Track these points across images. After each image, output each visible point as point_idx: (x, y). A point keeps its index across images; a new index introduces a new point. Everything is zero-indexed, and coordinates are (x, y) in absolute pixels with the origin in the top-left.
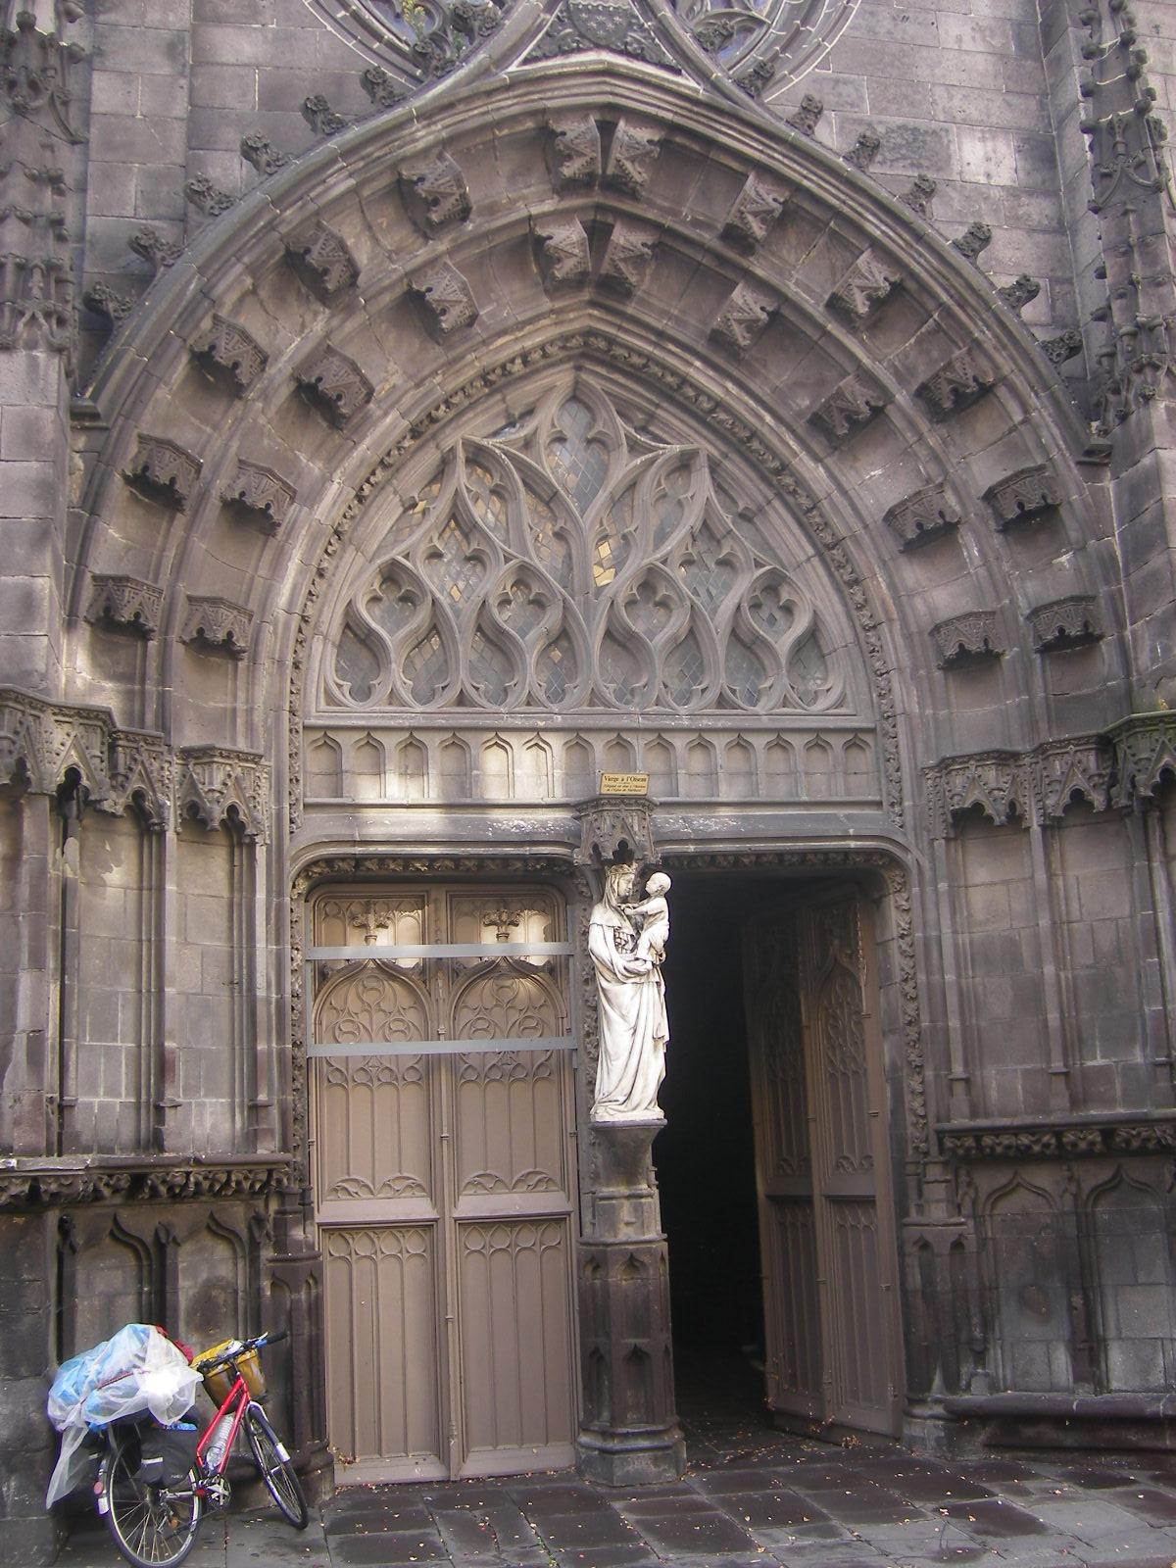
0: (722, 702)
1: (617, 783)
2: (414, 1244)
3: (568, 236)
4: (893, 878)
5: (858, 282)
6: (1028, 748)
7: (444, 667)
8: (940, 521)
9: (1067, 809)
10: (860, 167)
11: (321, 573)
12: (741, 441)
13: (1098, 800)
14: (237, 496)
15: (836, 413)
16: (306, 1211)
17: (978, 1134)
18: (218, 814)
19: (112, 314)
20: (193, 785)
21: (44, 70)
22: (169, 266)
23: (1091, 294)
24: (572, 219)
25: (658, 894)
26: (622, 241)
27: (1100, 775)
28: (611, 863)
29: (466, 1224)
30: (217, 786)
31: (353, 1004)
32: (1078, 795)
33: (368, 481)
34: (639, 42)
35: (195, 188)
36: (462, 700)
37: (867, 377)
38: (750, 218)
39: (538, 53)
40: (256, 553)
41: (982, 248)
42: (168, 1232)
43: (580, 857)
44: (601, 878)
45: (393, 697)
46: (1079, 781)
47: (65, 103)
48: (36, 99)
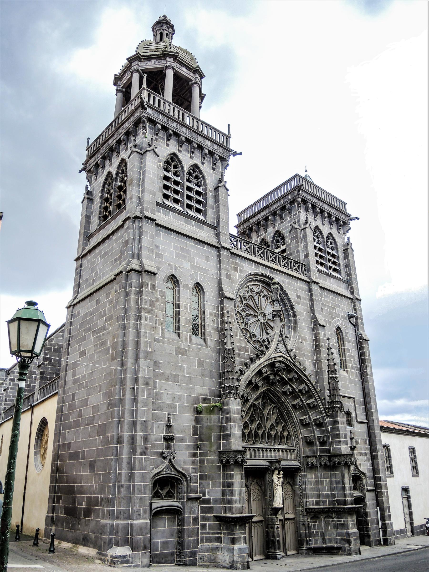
3: (272, 377)
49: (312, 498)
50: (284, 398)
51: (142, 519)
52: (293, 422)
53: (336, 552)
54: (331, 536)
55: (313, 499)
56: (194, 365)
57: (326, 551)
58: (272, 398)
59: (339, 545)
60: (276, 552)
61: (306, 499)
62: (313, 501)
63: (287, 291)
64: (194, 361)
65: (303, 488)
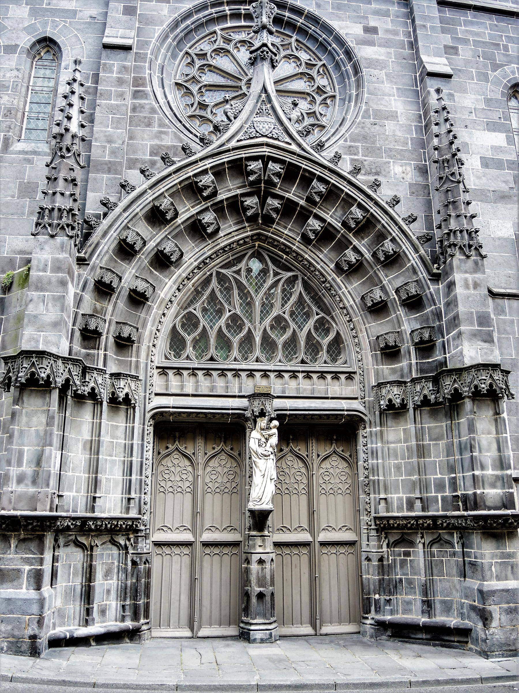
0: (303, 362)
3: (251, 201)
6: (409, 380)
11: (164, 314)
12: (312, 271)
17: (388, 518)
18: (122, 395)
21: (72, 144)
23: (437, 219)
25: (274, 427)
27: (433, 390)
28: (258, 417)
29: (206, 544)
30: (122, 386)
31: (170, 464)
32: (425, 396)
36: (212, 359)
37: (356, 250)
39: (243, 138)
41: (396, 204)
43: (248, 414)
44: (255, 422)
45: (188, 358)
46: (426, 392)
47: (79, 155)
49: (397, 491)
52: (344, 308)
53: (458, 642)
54: (448, 596)
55: (401, 495)
56: (10, 193)
57: (428, 637)
59: (467, 621)
60: (251, 624)
61: (379, 494)
62: (400, 499)
63: (327, 21)
64: (11, 185)
65: (370, 466)
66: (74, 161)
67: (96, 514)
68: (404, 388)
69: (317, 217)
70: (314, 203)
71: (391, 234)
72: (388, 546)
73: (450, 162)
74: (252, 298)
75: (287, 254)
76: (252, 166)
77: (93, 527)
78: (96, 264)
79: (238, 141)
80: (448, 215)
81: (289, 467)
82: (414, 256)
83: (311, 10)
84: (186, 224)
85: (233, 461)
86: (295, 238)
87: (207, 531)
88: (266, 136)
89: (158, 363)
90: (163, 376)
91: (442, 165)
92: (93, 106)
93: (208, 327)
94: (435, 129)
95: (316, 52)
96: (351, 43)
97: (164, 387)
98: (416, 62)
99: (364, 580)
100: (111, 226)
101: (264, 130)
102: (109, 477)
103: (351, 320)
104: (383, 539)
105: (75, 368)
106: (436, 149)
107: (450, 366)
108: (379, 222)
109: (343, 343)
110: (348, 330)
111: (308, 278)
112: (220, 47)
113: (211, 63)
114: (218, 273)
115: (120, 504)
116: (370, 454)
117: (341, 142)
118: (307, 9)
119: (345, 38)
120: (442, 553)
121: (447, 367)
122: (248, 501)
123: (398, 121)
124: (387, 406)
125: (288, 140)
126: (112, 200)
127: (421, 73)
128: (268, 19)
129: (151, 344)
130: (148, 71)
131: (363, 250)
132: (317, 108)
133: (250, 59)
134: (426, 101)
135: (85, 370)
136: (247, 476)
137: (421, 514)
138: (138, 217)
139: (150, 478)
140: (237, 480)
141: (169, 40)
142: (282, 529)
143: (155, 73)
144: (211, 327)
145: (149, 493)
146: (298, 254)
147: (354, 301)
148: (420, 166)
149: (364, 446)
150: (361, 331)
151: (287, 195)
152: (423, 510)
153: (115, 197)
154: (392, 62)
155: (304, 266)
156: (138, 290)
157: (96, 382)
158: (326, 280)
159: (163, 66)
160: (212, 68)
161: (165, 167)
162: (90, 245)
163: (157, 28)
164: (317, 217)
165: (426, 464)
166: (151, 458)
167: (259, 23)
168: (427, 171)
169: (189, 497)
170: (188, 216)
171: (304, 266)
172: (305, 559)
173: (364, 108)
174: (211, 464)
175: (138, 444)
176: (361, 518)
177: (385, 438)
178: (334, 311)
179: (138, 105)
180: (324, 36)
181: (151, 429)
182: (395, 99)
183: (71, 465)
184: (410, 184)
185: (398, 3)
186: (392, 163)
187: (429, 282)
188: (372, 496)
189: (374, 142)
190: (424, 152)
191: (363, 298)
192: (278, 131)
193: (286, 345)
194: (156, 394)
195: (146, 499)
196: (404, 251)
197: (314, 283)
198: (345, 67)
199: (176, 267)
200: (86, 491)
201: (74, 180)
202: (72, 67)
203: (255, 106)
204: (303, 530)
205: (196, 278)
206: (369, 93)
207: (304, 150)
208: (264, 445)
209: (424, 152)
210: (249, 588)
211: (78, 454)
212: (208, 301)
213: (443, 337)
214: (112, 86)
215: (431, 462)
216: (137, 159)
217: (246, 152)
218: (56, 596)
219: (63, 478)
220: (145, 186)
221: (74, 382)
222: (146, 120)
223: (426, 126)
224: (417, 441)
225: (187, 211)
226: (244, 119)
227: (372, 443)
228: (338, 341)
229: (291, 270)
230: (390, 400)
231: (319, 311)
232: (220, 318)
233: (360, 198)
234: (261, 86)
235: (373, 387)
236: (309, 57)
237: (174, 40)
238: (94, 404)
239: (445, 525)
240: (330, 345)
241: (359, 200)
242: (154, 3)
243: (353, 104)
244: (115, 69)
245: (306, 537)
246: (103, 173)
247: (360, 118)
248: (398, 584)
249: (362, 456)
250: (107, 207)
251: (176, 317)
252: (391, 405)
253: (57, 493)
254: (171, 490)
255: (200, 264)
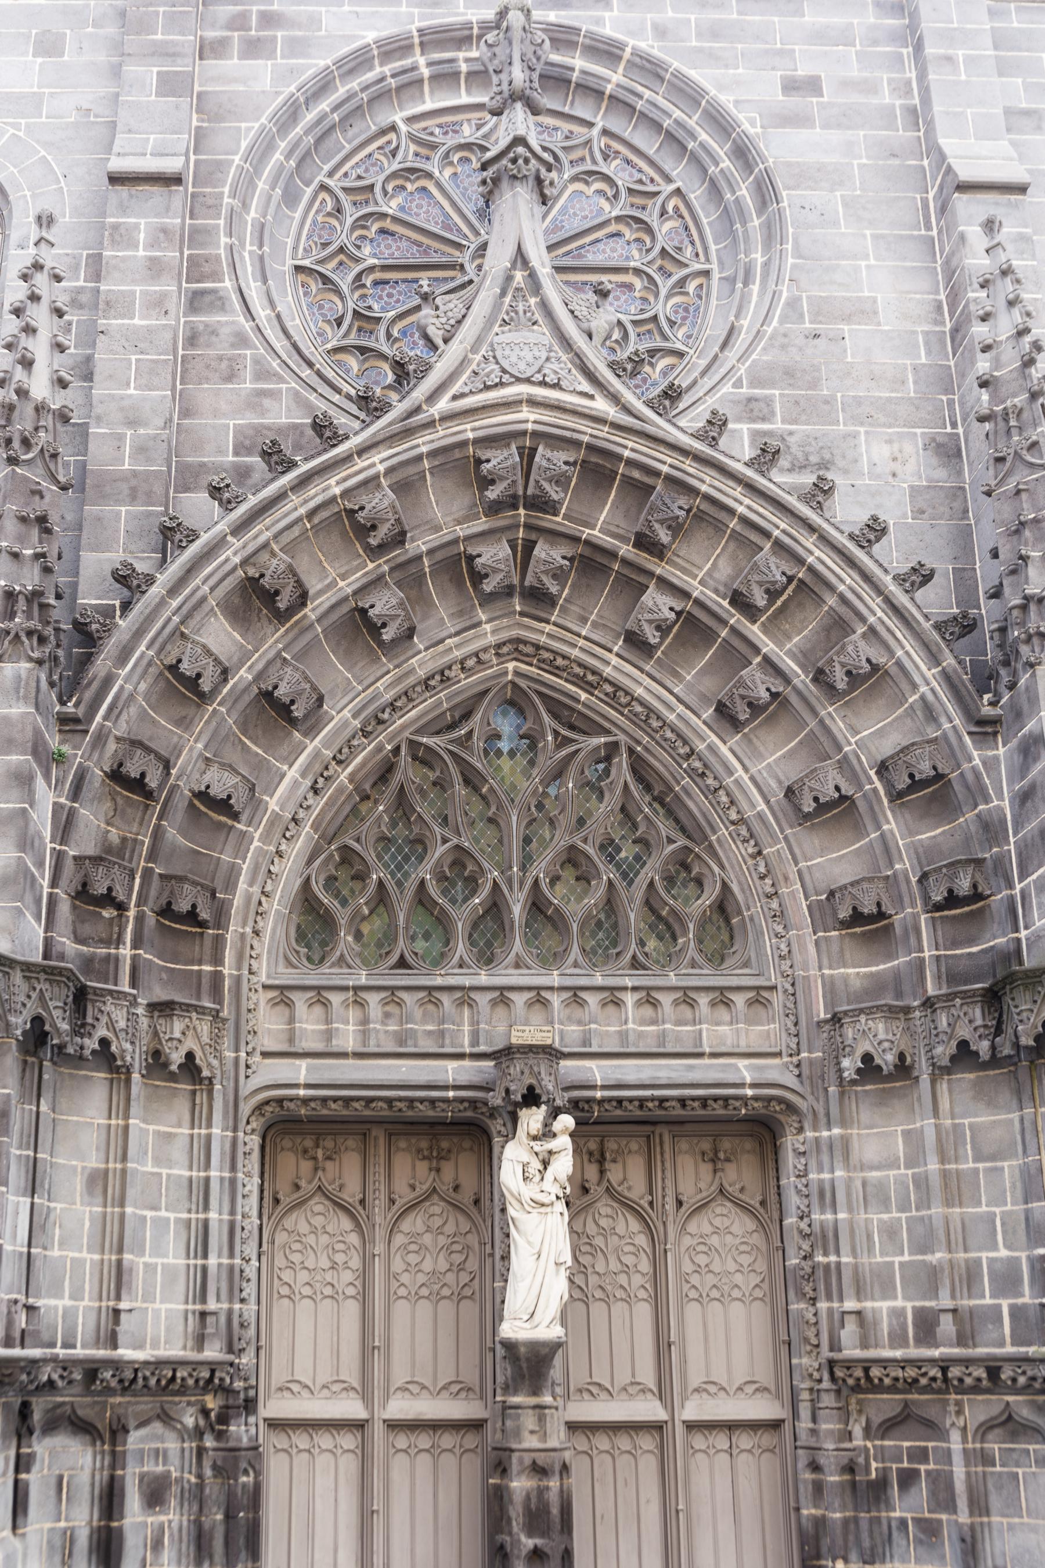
1: (525, 1035)
2: (348, 1441)
4: (790, 1122)
5: (756, 578)
6: (916, 1003)
7: (390, 936)
8: (837, 795)
9: (953, 1058)
10: (762, 473)
11: (279, 854)
13: (983, 1047)
14: (203, 788)
15: (738, 701)
16: (250, 1405)
17: (867, 1365)
18: (177, 1058)
19: (96, 635)
20: (156, 1034)
21: (37, 429)
22: (144, 593)
24: (500, 539)
25: (563, 1132)
26: (543, 555)
29: (394, 1426)
30: (177, 1034)
31: (303, 1227)
32: (963, 1045)
33: (322, 775)
34: (556, 373)
35: (167, 524)
36: (402, 963)
37: (769, 664)
38: (657, 526)
39: (466, 390)
40: (222, 838)
42: (119, 1420)
43: (496, 1099)
44: (515, 1119)
46: (964, 1032)
48: (26, 453)
49: (888, 1291)
50: (647, 681)
51: (951, 1464)
52: (742, 821)
55: (899, 1303)
58: (578, 701)
61: (841, 1300)
63: (693, 74)
65: (816, 1228)
66: (41, 471)
67: (121, 1351)
68: (902, 1024)
69: (665, 584)
70: (657, 550)
71: (863, 619)
72: (868, 1433)
73: (1025, 415)
74: (500, 807)
75: (589, 687)
76: (494, 462)
77: (114, 1383)
78: (105, 731)
79: (455, 398)
80: (1021, 557)
81: (603, 1232)
82: (929, 675)
83: (642, 45)
84: (327, 622)
85: (461, 1219)
86: (609, 645)
87: (399, 1394)
88: (528, 381)
89: (268, 977)
90: (281, 1008)
91: (1001, 424)
92: (92, 335)
93: (391, 886)
94: (979, 331)
95: (657, 158)
96: (748, 123)
97: (285, 1036)
98: (926, 162)
99: (804, 1521)
100: (138, 634)
101: (522, 366)
102: (153, 1260)
103: (760, 853)
104: (854, 1416)
105: (56, 989)
106: (984, 384)
107: (1029, 962)
108: (831, 588)
109: (739, 913)
110: (752, 880)
111: (646, 749)
112: (408, 165)
113: (385, 209)
114: (412, 743)
115: (181, 1328)
116: (815, 1199)
117: (727, 388)
118: (632, 42)
119: (734, 111)
120: (1015, 1456)
121: (1021, 963)
122: (501, 1320)
123: (879, 324)
124: (859, 1071)
125: (585, 386)
126: (141, 567)
127: (941, 188)
128: (527, 72)
129: (248, 930)
130: (224, 240)
131: (790, 665)
132: (660, 306)
133: (484, 182)
134: (954, 263)
135: (81, 997)
136: (498, 1257)
137: (956, 1351)
138: (206, 608)
139: (254, 1263)
140: (473, 1264)
141: (278, 156)
142: (592, 1390)
143: (243, 245)
144: (399, 884)
145: (253, 1299)
146: (617, 687)
147: (768, 802)
148: (939, 439)
149: (798, 1176)
150: (786, 879)
151: (586, 533)
152: (962, 1340)
153: (150, 563)
154: (861, 166)
155: (634, 716)
156: (212, 792)
157: (111, 1025)
158: (692, 751)
159: (263, 225)
160: (387, 224)
161: (270, 476)
162: (89, 684)
163: (243, 125)
164: (665, 584)
165: (967, 1222)
166: (255, 1213)
167: (505, 87)
168: (959, 450)
169: (352, 1308)
170: (333, 600)
171: (634, 716)
172: (649, 1465)
173: (785, 295)
174: (406, 1225)
175: (222, 1179)
176: (795, 1361)
177: (855, 1157)
178: (715, 832)
179: (201, 327)
180: (677, 114)
181: (255, 1141)
182: (868, 267)
183: (57, 1231)
184: (911, 487)
185: (877, 5)
186: (863, 437)
187: (967, 739)
188: (823, 1305)
189: (814, 384)
190: (950, 403)
191: (790, 792)
192: (561, 366)
193: (592, 925)
194: (265, 1055)
195: (246, 1316)
196: (899, 664)
197: (661, 761)
198: (734, 192)
199: (305, 734)
200: (96, 1295)
201: (42, 520)
202: (34, 233)
203: (497, 306)
204: (643, 1391)
205: (359, 759)
206: (798, 254)
207: (627, 410)
208: (538, 1177)
209: (950, 403)
210: (508, 1539)
211: (74, 1203)
212: (391, 818)
213: (1010, 886)
214: (134, 282)
215: (980, 1217)
216: (202, 465)
217: (477, 424)
218: (25, 1556)
219: (37, 1264)
220: (222, 527)
221: (54, 1025)
222: (224, 365)
223: (955, 331)
224: (942, 1161)
225: (329, 587)
226: (471, 339)
227: (821, 1170)
228: (724, 907)
229: (608, 732)
230: (867, 1058)
231: (673, 835)
232: (421, 859)
233: (779, 526)
234: (510, 250)
235: (819, 1024)
236: (637, 176)
237: (288, 156)
238: (112, 1080)
239: (1022, 1380)
240: (703, 923)
241: (776, 533)
242: (236, 60)
243: (755, 288)
244: (142, 236)
245: (650, 1410)
246: (119, 502)
247: (775, 323)
248: (895, 1534)
249: (793, 1201)
250: (129, 588)
251: (310, 862)
252: (869, 1068)
253: (22, 1298)
254: (307, 1291)
255: (365, 723)
